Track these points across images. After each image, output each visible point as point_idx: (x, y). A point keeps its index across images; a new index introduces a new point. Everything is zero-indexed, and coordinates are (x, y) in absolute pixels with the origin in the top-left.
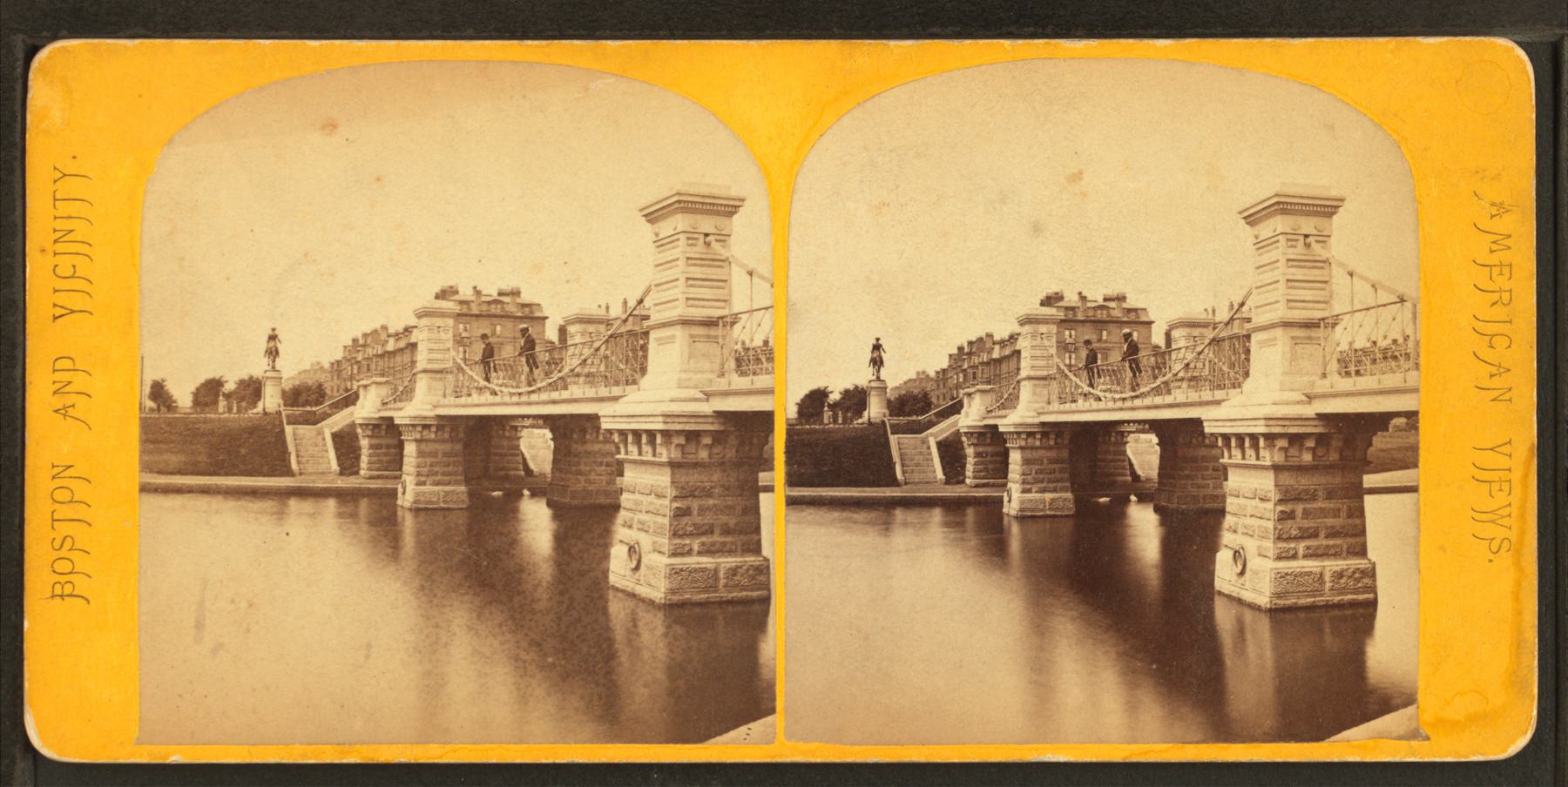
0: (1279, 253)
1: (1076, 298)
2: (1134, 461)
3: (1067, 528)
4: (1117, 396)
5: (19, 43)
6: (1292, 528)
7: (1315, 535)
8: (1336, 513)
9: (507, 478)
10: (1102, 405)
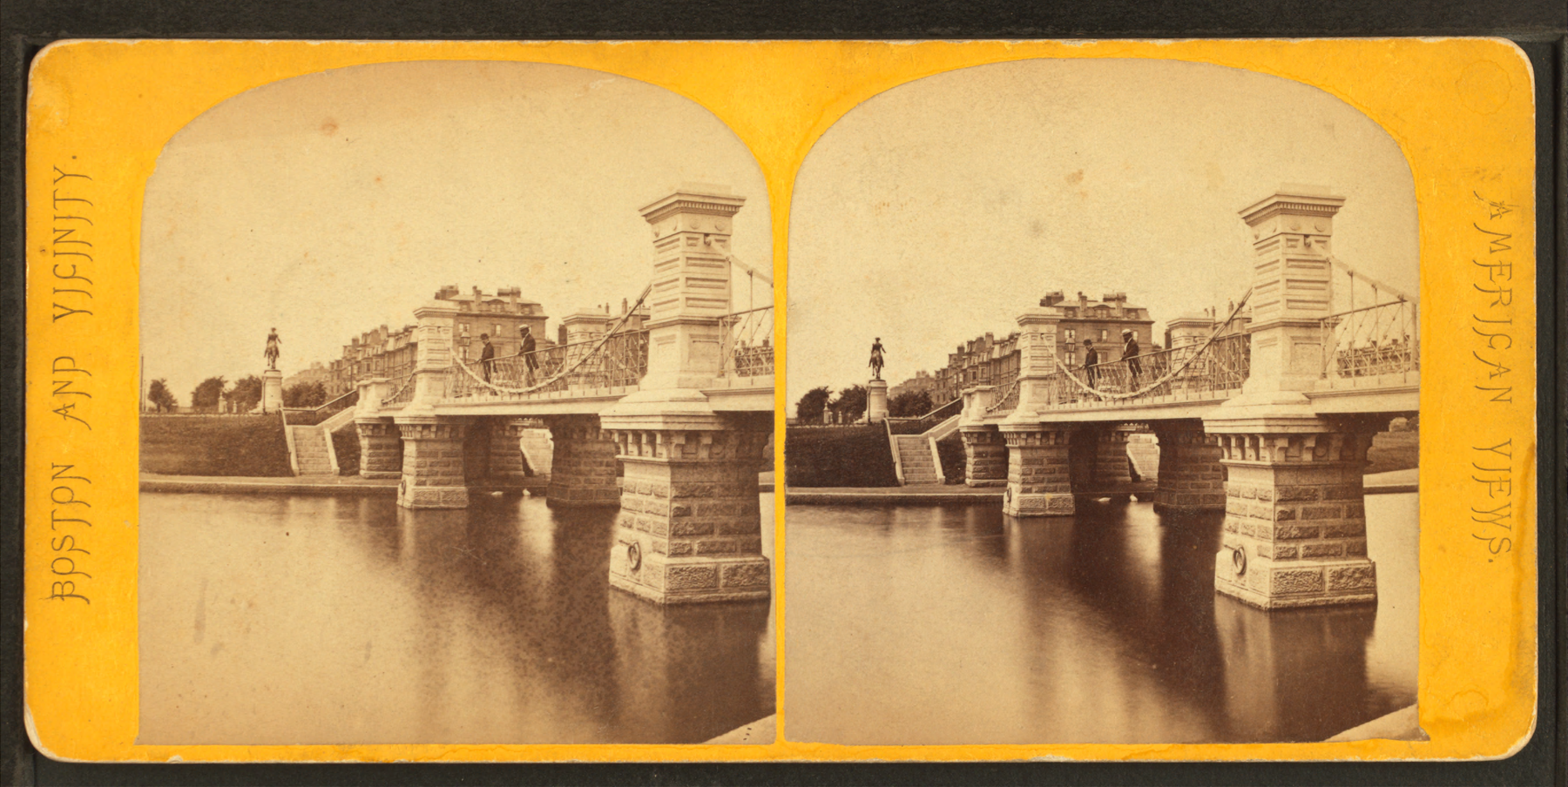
0: (1279, 253)
1: (1076, 298)
2: (1134, 461)
3: (1067, 528)
4: (1117, 396)
5: (19, 43)
6: (1292, 528)
7: (1315, 535)
8: (1336, 513)
9: (507, 478)
10: (1102, 405)
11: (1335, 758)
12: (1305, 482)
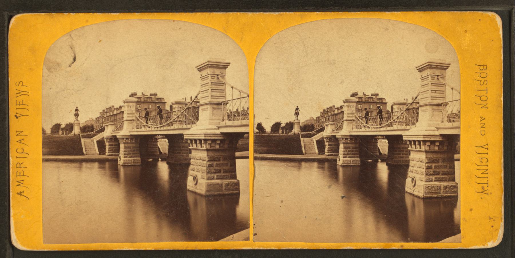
0: (429, 80)
1: (141, 94)
3: (139, 169)
4: (375, 127)
5: (6, 14)
6: (212, 169)
8: (445, 167)
9: (154, 155)
10: (370, 130)
11: (459, 246)
12: (216, 155)
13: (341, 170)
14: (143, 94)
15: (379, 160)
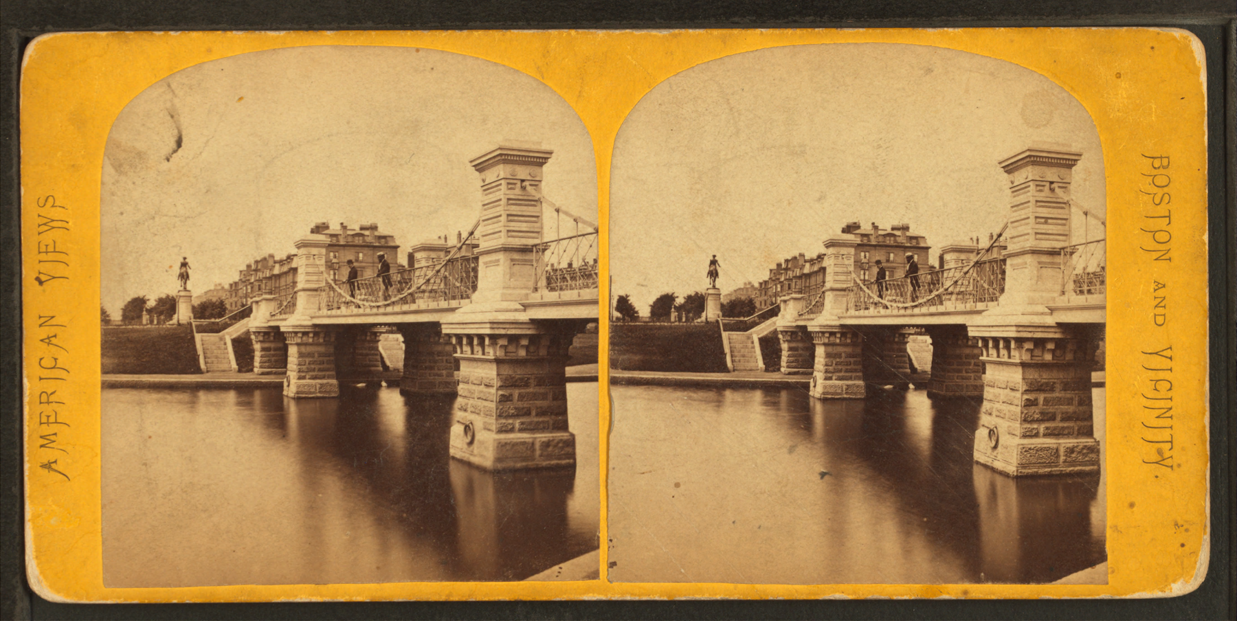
0: (1032, 193)
1: (339, 227)
4: (901, 305)
5: (14, 34)
6: (510, 408)
7: (1053, 418)
8: (1069, 402)
9: (370, 372)
11: (1103, 593)
12: (520, 372)
13: (818, 408)
14: (344, 227)
15: (911, 386)
